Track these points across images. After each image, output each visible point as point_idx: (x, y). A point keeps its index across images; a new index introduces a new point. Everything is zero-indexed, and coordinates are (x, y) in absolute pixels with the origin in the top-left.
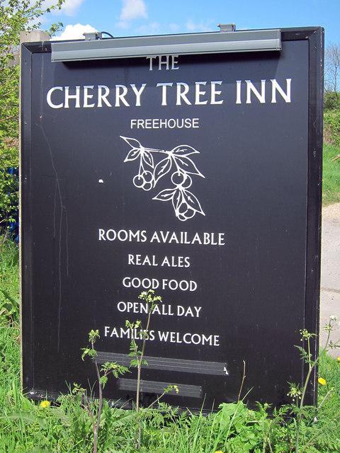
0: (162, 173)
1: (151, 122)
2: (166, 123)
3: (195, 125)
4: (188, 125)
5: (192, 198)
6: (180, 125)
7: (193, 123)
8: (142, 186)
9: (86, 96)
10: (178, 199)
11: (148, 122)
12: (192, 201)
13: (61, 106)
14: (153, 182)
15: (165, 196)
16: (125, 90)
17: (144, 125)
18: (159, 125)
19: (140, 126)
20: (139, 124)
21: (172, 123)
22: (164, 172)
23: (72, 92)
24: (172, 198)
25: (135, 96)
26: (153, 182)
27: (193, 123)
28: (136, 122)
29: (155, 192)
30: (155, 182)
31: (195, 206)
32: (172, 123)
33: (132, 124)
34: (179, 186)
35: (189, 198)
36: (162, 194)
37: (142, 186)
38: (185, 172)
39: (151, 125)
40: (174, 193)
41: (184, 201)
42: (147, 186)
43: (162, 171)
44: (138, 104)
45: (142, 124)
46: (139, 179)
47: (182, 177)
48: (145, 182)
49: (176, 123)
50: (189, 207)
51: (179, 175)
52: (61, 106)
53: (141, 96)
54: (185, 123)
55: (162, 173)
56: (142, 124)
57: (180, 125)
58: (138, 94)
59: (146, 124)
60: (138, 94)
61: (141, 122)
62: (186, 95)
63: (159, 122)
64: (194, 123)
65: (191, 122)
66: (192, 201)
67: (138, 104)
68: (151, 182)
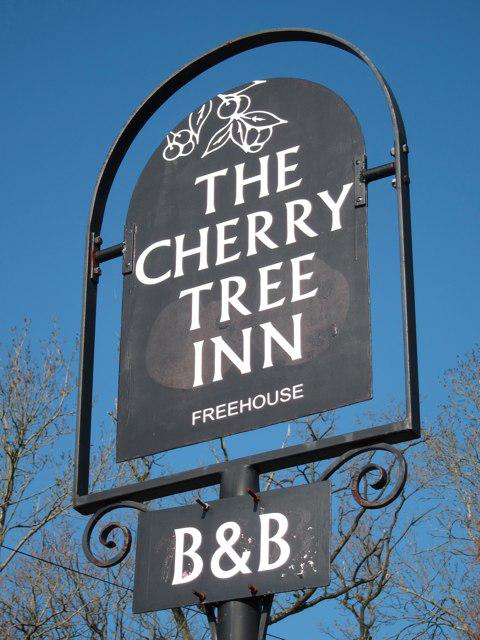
0: (201, 120)
1: (226, 408)
2: (251, 404)
3: (297, 394)
4: (286, 392)
5: (259, 115)
6: (273, 400)
7: (294, 393)
8: (180, 154)
9: (222, 242)
10: (240, 130)
11: (221, 409)
12: (260, 119)
13: (167, 275)
14: (194, 138)
15: (219, 141)
16: (307, 206)
17: (214, 415)
18: (238, 410)
19: (208, 418)
20: (205, 416)
21: (259, 402)
22: (205, 115)
23: (192, 242)
24: (231, 136)
25: (329, 213)
26: (194, 138)
27: (294, 393)
28: (201, 415)
29: (201, 147)
30: (197, 136)
31: (270, 120)
32: (259, 402)
33: (194, 418)
34: (235, 116)
35: (255, 119)
36: (214, 141)
37: (180, 154)
38: (234, 95)
39: (226, 413)
40: (230, 129)
41: (249, 127)
42: (186, 150)
43: (201, 117)
44: (336, 225)
45: (210, 415)
46: (172, 149)
47: (233, 104)
48: (182, 147)
49: (266, 399)
50: (259, 129)
51: (228, 104)
52: (167, 275)
53: (343, 211)
54: (280, 396)
55: (201, 120)
56: (210, 415)
57: (273, 400)
58: (335, 207)
59: (218, 412)
60: (335, 207)
61: (209, 412)
62: (307, 221)
63: (238, 405)
64: (295, 392)
65: (291, 393)
66: (260, 119)
67: (336, 225)
68: (191, 140)
